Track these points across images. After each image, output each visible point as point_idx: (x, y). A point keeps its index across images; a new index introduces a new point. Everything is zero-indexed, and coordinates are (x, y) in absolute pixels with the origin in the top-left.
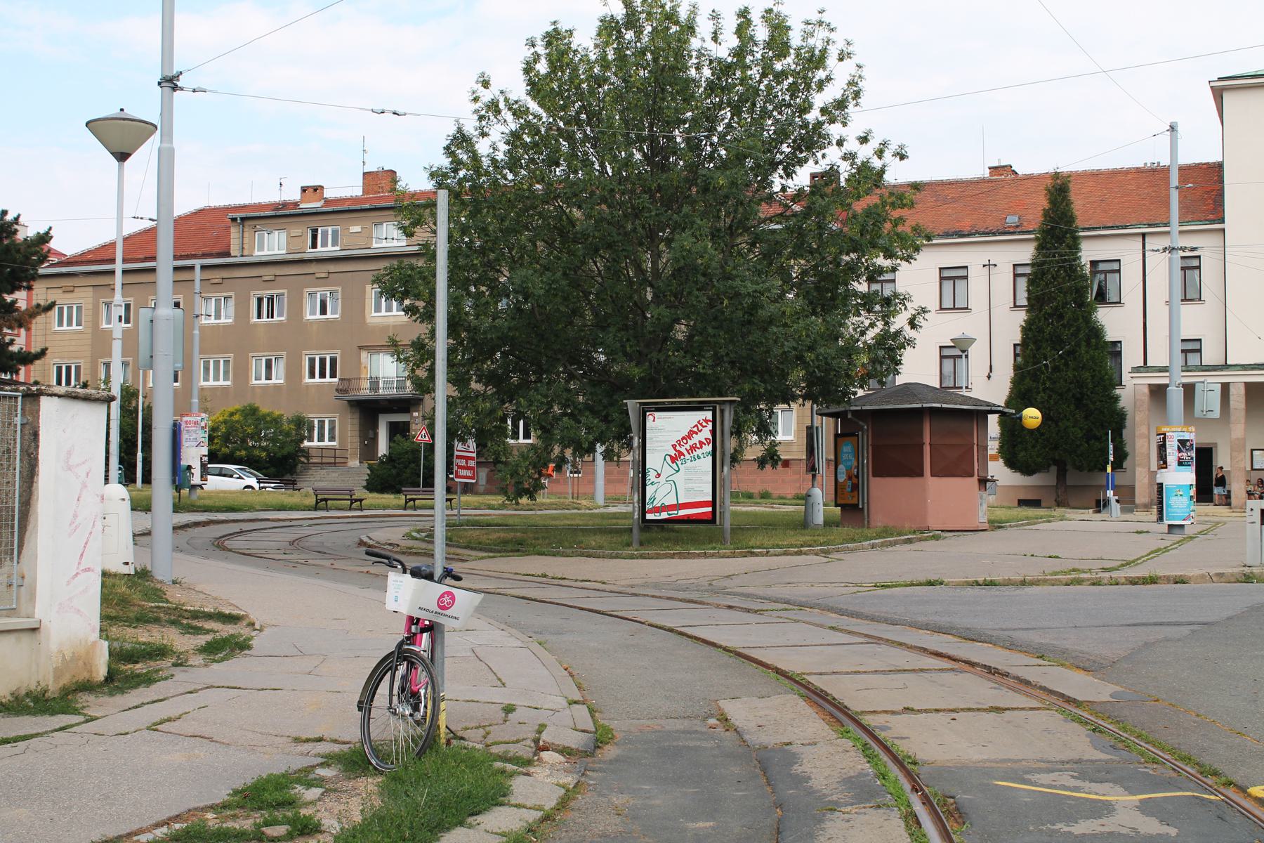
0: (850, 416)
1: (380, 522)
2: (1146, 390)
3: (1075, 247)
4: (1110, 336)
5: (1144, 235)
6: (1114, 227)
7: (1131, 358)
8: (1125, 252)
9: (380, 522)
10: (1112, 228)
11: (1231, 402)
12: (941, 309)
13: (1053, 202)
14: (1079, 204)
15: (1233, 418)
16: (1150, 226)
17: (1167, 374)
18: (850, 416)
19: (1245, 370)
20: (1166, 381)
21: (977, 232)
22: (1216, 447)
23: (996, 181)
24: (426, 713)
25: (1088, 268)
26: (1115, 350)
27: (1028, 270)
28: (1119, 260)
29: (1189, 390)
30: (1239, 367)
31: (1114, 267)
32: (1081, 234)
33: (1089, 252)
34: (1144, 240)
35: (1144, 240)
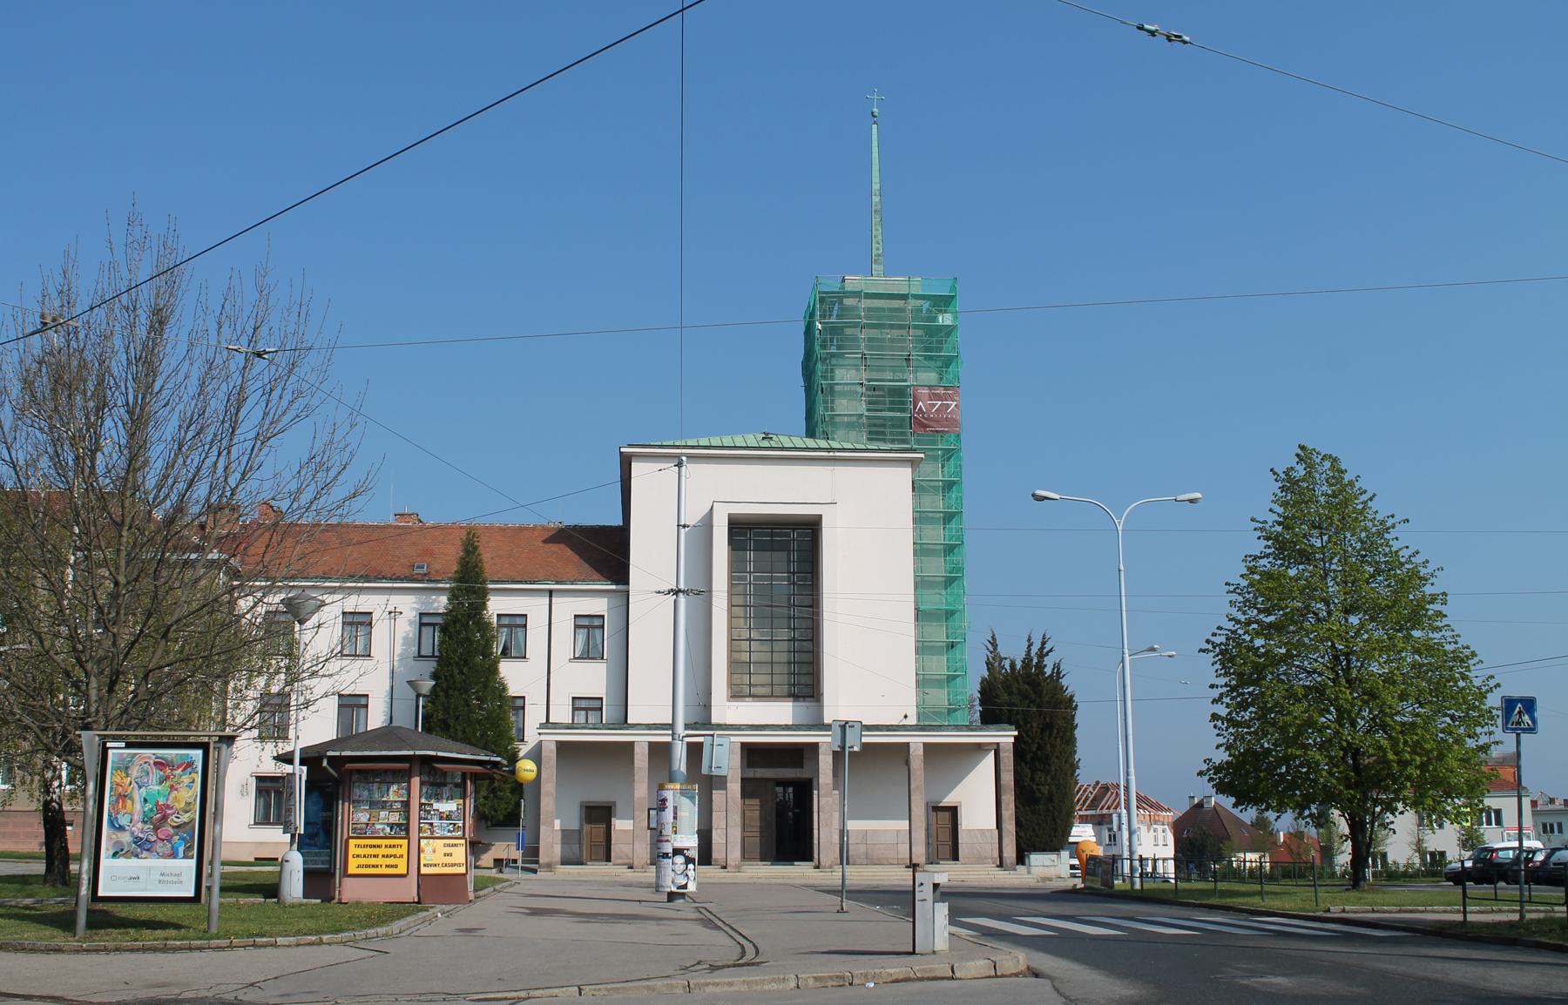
0: (325, 763)
1: (371, 846)
2: (554, 747)
3: (483, 595)
4: (513, 691)
5: (551, 592)
6: (523, 577)
7: (533, 717)
8: (533, 607)
9: (371, 846)
10: (520, 582)
11: (636, 761)
12: (420, 656)
13: (467, 552)
14: (488, 557)
15: (636, 777)
16: (557, 583)
17: (830, 733)
18: (325, 763)
19: (650, 729)
20: (669, 739)
21: (384, 578)
22: (615, 806)
23: (399, 527)
24: (1348, 912)
25: (495, 620)
26: (518, 705)
27: (439, 620)
28: (526, 615)
29: (695, 751)
30: (643, 727)
31: (518, 623)
32: (490, 586)
33: (497, 606)
34: (551, 596)
35: (551, 596)
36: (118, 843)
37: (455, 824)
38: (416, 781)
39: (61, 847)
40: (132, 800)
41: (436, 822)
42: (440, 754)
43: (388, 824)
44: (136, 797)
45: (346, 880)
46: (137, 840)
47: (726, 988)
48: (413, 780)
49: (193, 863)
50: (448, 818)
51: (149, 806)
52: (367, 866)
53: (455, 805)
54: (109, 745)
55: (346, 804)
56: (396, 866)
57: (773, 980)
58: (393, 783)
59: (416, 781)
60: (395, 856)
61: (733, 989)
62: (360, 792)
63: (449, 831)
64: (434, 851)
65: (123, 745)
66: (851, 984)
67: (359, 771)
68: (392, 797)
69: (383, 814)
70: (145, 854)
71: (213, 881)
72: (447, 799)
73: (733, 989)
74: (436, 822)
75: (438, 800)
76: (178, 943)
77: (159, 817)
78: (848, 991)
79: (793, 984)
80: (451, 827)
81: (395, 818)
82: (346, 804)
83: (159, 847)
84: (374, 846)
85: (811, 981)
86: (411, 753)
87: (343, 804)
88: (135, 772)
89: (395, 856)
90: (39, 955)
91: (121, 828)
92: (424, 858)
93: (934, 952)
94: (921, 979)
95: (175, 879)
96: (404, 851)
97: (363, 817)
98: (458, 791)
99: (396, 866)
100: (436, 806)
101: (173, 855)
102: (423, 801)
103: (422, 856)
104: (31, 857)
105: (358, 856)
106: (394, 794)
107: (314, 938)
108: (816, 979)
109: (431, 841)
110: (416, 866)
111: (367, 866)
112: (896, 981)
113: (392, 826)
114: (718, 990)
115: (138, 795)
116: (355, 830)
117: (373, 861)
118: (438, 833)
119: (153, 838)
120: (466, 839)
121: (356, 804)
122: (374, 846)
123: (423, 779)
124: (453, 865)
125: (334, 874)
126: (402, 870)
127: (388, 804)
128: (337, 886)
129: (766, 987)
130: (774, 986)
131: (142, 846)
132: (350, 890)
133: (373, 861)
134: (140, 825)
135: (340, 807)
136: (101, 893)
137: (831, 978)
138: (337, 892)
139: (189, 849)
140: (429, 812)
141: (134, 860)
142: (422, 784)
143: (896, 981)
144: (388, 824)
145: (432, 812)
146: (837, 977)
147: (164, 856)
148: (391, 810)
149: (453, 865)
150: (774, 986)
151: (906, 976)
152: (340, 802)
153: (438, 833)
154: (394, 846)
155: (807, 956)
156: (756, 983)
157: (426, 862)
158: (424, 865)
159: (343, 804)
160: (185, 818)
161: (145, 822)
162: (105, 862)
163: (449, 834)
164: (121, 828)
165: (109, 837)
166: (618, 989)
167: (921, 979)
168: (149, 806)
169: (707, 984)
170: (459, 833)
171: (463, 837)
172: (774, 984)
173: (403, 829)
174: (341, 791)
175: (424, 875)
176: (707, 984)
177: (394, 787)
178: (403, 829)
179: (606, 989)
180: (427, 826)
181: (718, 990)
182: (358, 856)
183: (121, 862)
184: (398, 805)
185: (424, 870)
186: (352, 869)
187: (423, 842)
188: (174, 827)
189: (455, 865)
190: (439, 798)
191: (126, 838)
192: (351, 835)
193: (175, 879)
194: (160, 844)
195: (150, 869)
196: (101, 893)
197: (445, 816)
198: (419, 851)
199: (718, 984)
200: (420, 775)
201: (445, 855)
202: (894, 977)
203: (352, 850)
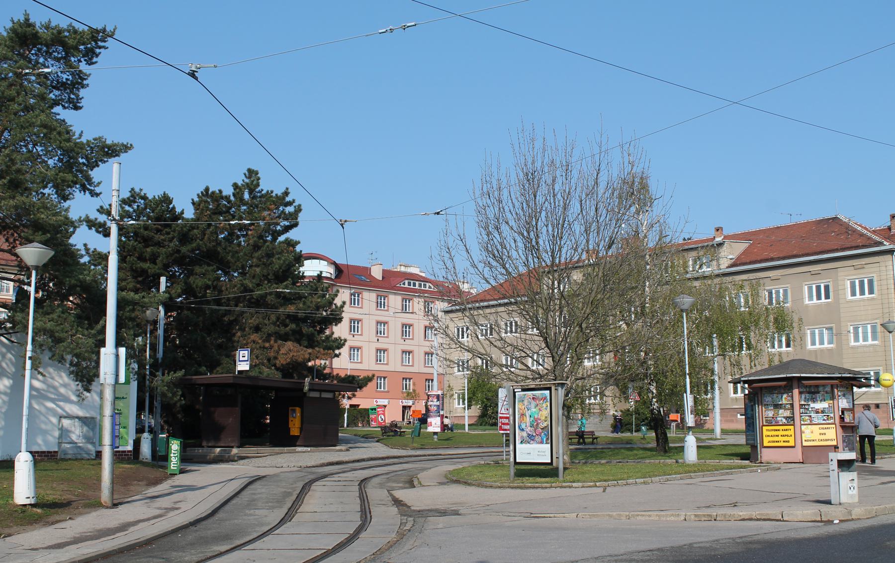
36: (522, 437)
37: (828, 416)
38: (796, 392)
39: (662, 433)
40: (526, 416)
41: (813, 415)
42: (802, 375)
43: (784, 417)
44: (527, 414)
45: (763, 450)
46: (529, 435)
47: (647, 518)
48: (794, 391)
49: (549, 446)
50: (823, 412)
51: (532, 419)
52: (774, 442)
53: (827, 404)
54: (515, 390)
55: (760, 407)
56: (788, 442)
57: (672, 515)
58: (784, 393)
59: (796, 392)
60: (788, 436)
61: (651, 518)
62: (768, 399)
63: (824, 420)
64: (812, 432)
65: (520, 390)
66: (715, 520)
67: (766, 387)
68: (784, 402)
69: (781, 411)
70: (532, 442)
71: (559, 455)
72: (821, 401)
73: (651, 518)
74: (813, 415)
75: (814, 402)
76: (530, 485)
77: (535, 424)
78: (713, 523)
79: (683, 518)
80: (825, 418)
81: (788, 413)
82: (760, 407)
83: (538, 439)
84: (776, 430)
85: (693, 517)
86: (785, 376)
87: (758, 407)
88: (526, 402)
89: (788, 436)
90: (473, 487)
91: (523, 430)
92: (805, 436)
93: (840, 504)
94: (758, 520)
95: (543, 454)
96: (792, 432)
97: (770, 414)
98: (828, 396)
99: (788, 442)
100: (812, 405)
101: (542, 442)
102: (803, 403)
103: (803, 435)
104: (736, 432)
105: (768, 436)
106: (785, 400)
107: (592, 484)
108: (696, 516)
109: (809, 426)
110: (800, 442)
111: (774, 442)
112: (743, 520)
113: (786, 418)
114: (643, 518)
115: (528, 413)
116: (767, 421)
117: (776, 439)
118: (815, 421)
119: (534, 434)
120: (835, 424)
121: (766, 406)
122: (776, 430)
123: (801, 390)
124: (827, 440)
125: (757, 446)
126: (792, 444)
127: (783, 406)
128: (759, 453)
129: (668, 519)
130: (673, 518)
131: (531, 438)
132: (766, 455)
133: (776, 439)
134: (529, 428)
135: (757, 408)
136: (517, 461)
137: (704, 516)
138: (759, 457)
139: (547, 439)
140: (807, 409)
141: (528, 445)
142: (800, 393)
143: (743, 520)
144: (784, 417)
145: (810, 409)
146: (708, 515)
147: (538, 443)
148: (785, 409)
149: (827, 440)
150: (673, 518)
151: (750, 517)
152: (757, 405)
153: (815, 421)
154: (787, 430)
155: (807, 502)
156: (663, 516)
157: (806, 439)
158: (805, 441)
159: (758, 407)
160: (545, 424)
161: (531, 427)
162: (518, 446)
163: (824, 422)
164: (523, 430)
165: (519, 434)
166: (594, 515)
167: (758, 520)
168: (532, 419)
169: (638, 515)
170: (832, 421)
171: (834, 424)
172: (672, 517)
173: (791, 420)
174: (756, 399)
175: (804, 446)
176: (638, 515)
177: (785, 396)
178: (791, 420)
179: (589, 515)
180: (807, 418)
181: (643, 518)
182: (768, 436)
183: (524, 445)
184: (789, 406)
185: (805, 444)
186: (766, 444)
187: (803, 427)
188: (542, 429)
189: (828, 440)
190: (814, 400)
191: (525, 434)
192: (765, 424)
193: (543, 454)
194: (537, 437)
195: (534, 449)
196: (517, 461)
197: (820, 411)
198: (802, 432)
199: (643, 515)
200: (798, 388)
201: (820, 434)
202: (742, 518)
203: (765, 433)
